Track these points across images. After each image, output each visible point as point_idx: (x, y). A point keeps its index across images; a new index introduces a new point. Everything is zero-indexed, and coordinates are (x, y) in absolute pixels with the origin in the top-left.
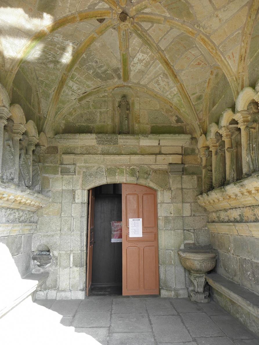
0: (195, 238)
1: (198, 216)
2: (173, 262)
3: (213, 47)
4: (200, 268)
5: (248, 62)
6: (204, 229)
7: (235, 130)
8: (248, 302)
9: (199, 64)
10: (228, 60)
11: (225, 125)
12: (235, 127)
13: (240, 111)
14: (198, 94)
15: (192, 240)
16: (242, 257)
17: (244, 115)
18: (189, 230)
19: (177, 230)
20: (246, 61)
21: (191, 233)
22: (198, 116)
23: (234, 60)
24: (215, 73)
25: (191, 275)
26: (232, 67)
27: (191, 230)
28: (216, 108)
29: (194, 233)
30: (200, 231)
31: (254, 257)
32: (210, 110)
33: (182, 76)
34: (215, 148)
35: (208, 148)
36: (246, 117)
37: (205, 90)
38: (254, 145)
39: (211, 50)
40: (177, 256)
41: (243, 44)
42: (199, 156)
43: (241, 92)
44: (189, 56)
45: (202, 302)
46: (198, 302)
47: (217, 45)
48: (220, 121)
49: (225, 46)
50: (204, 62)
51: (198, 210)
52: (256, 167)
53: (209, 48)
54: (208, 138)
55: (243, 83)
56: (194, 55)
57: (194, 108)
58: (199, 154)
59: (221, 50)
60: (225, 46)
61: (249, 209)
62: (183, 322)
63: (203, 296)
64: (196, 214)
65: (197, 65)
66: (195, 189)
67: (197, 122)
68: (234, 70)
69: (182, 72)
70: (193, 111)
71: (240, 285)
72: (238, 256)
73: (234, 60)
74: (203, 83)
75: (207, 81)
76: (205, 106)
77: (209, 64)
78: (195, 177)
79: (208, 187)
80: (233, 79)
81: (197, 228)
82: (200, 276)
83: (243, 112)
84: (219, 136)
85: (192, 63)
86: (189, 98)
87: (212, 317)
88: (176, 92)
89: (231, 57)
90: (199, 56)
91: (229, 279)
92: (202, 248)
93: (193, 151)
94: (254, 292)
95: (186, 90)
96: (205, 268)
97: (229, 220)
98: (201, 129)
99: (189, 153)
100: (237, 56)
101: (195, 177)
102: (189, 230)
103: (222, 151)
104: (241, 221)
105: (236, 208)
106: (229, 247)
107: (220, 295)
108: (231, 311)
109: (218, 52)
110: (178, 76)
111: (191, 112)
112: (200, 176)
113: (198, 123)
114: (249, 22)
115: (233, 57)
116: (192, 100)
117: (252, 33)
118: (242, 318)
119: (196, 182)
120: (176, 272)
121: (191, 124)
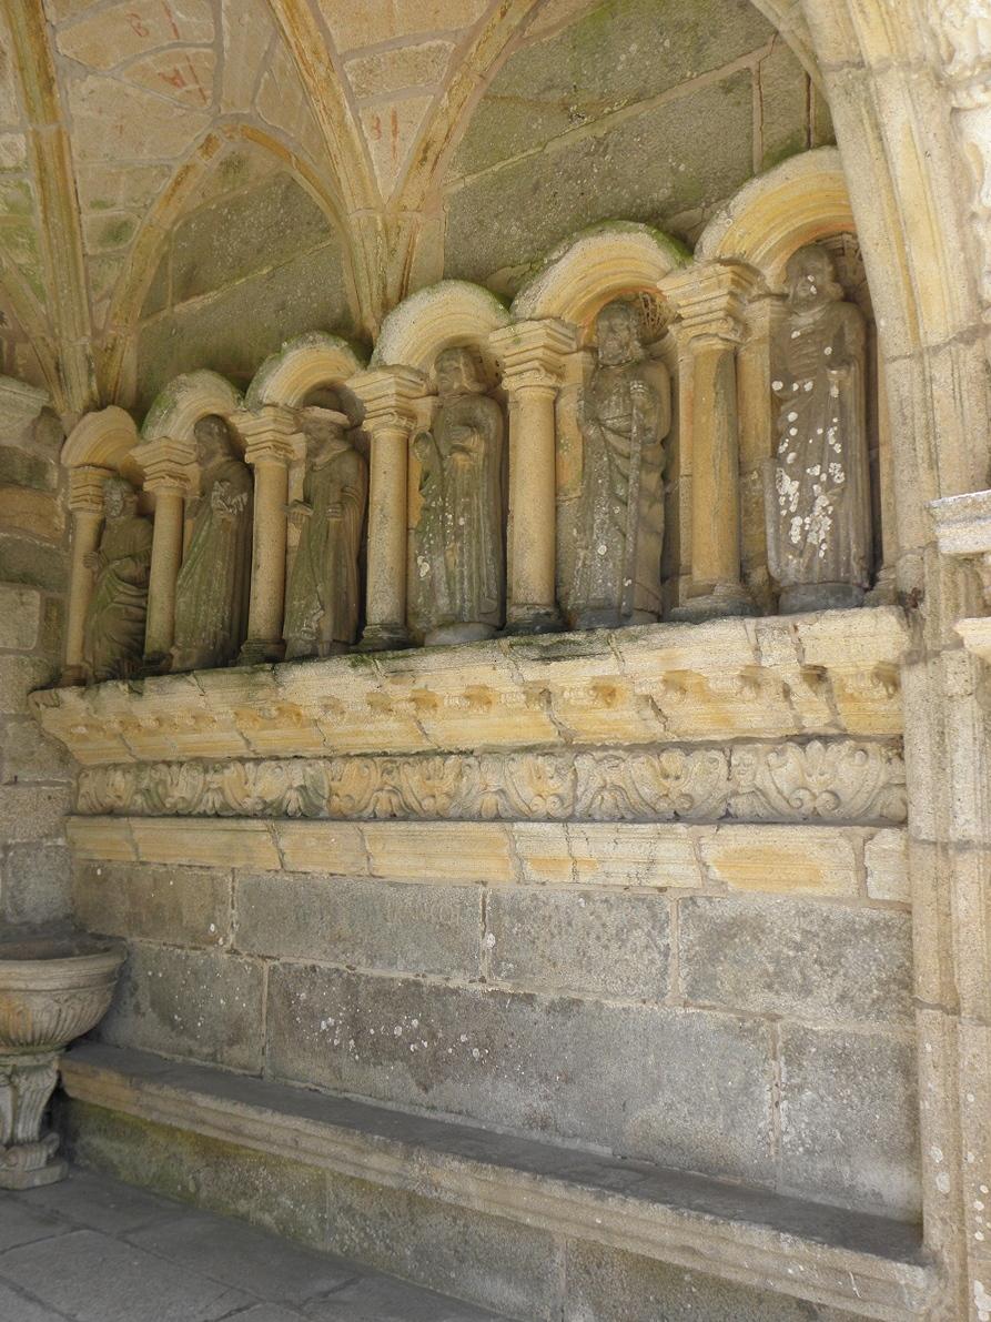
1: (29, 785)
3: (322, 48)
4: (52, 1026)
5: (456, 182)
6: (49, 844)
7: (331, 432)
8: (376, 1137)
9: (173, 79)
10: (366, 135)
11: (278, 398)
12: (332, 423)
13: (394, 366)
14: (117, 213)
16: (292, 960)
17: (404, 386)
20: (438, 170)
22: (90, 310)
23: (394, 148)
24: (225, 149)
26: (377, 173)
28: (205, 310)
30: (33, 852)
31: (368, 957)
32: (152, 307)
33: (80, 99)
34: (177, 483)
35: (132, 480)
36: (405, 397)
37: (151, 204)
38: (461, 519)
39: (309, 57)
41: (445, 102)
42: (59, 502)
43: (422, 294)
44: (150, 21)
45: (37, 1182)
46: (14, 1190)
47: (339, 51)
48: (262, 378)
49: (371, 71)
50: (202, 85)
51: (32, 753)
52: (462, 608)
53: (305, 44)
54: (153, 432)
55: (409, 253)
56: (176, 31)
57: (86, 269)
58: (63, 490)
59: (349, 77)
60: (371, 71)
61: (367, 767)
62: (31, 1298)
63: (39, 1156)
64: (25, 777)
65: (164, 78)
66: (27, 654)
67: (84, 340)
68: (385, 186)
69: (83, 81)
70: (78, 280)
71: (261, 1077)
72: (264, 958)
73: (394, 148)
74: (154, 173)
75: (175, 173)
76: (128, 278)
77: (217, 99)
78: (34, 598)
79: (112, 652)
80: (372, 221)
81: (19, 840)
82: (35, 1063)
83: (405, 375)
84: (217, 438)
85: (149, 60)
86: (75, 213)
87: (130, 1237)
88: (17, 159)
89: (383, 128)
90: (197, 46)
91: (192, 1059)
92: (34, 932)
93: (37, 469)
94: (348, 1095)
95: (73, 172)
96: (73, 1025)
97: (226, 806)
98: (94, 378)
99: (18, 478)
100: (410, 142)
101: (34, 598)
103: (230, 506)
104: (308, 815)
105: (278, 759)
106: (211, 919)
107: (133, 1130)
108: (203, 1194)
109: (334, 78)
110: (59, 89)
111: (70, 285)
112: (55, 595)
113: (84, 346)
114: (494, 26)
115: (395, 133)
116: (84, 229)
117: (493, 75)
118: (270, 1212)
119: (36, 623)
121: (43, 339)
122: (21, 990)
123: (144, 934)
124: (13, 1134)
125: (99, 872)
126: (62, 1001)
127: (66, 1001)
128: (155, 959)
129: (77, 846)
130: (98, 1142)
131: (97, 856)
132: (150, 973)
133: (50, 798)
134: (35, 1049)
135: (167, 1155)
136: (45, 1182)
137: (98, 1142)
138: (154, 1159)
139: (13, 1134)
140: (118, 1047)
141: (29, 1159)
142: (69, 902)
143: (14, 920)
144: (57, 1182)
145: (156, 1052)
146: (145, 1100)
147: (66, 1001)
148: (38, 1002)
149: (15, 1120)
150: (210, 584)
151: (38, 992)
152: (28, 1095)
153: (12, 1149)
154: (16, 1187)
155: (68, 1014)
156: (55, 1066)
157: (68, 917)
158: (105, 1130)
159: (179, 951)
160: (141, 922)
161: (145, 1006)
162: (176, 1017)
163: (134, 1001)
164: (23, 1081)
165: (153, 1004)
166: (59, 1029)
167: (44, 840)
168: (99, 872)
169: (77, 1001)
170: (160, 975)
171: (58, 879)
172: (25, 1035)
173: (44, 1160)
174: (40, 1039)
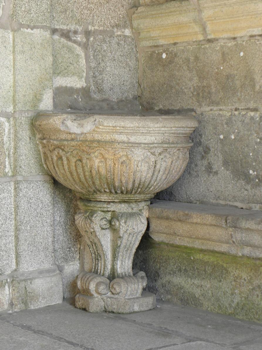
0: (89, 68)
2: (10, 163)
4: (150, 175)
6: (119, 33)
15: (80, 77)
18: (69, 31)
19: (28, 27)
21: (75, 46)
25: (93, 213)
27: (76, 32)
29: (85, 46)
30: (108, 39)
40: (28, 139)
45: (136, 308)
81: (96, 28)
82: (130, 211)
102: (71, 34)
120: (23, 205)
122: (124, 142)
123: (213, 103)
124: (113, 269)
125: (164, 56)
126: (157, 154)
127: (160, 154)
128: (227, 124)
129: (142, 35)
130: (178, 280)
131: (162, 42)
132: (222, 137)
134: (132, 197)
135: (251, 287)
136: (143, 309)
137: (178, 280)
138: (237, 291)
139: (113, 269)
140: (191, 202)
141: (129, 289)
142: (136, 85)
143: (97, 96)
144: (150, 310)
145: (231, 203)
146: (239, 236)
147: (160, 154)
148: (138, 154)
149: (115, 257)
151: (138, 145)
152: (126, 236)
153: (115, 280)
154: (121, 311)
155: (162, 165)
156: (146, 214)
157: (135, 98)
158: (185, 270)
159: (252, 114)
160: (209, 93)
161: (218, 164)
162: (251, 172)
163: (205, 162)
164: (123, 224)
165: (226, 163)
166: (154, 178)
167: (115, 30)
168: (164, 56)
169: (168, 156)
170: (233, 137)
171: (127, 64)
172: (127, 183)
173: (140, 291)
174: (138, 188)
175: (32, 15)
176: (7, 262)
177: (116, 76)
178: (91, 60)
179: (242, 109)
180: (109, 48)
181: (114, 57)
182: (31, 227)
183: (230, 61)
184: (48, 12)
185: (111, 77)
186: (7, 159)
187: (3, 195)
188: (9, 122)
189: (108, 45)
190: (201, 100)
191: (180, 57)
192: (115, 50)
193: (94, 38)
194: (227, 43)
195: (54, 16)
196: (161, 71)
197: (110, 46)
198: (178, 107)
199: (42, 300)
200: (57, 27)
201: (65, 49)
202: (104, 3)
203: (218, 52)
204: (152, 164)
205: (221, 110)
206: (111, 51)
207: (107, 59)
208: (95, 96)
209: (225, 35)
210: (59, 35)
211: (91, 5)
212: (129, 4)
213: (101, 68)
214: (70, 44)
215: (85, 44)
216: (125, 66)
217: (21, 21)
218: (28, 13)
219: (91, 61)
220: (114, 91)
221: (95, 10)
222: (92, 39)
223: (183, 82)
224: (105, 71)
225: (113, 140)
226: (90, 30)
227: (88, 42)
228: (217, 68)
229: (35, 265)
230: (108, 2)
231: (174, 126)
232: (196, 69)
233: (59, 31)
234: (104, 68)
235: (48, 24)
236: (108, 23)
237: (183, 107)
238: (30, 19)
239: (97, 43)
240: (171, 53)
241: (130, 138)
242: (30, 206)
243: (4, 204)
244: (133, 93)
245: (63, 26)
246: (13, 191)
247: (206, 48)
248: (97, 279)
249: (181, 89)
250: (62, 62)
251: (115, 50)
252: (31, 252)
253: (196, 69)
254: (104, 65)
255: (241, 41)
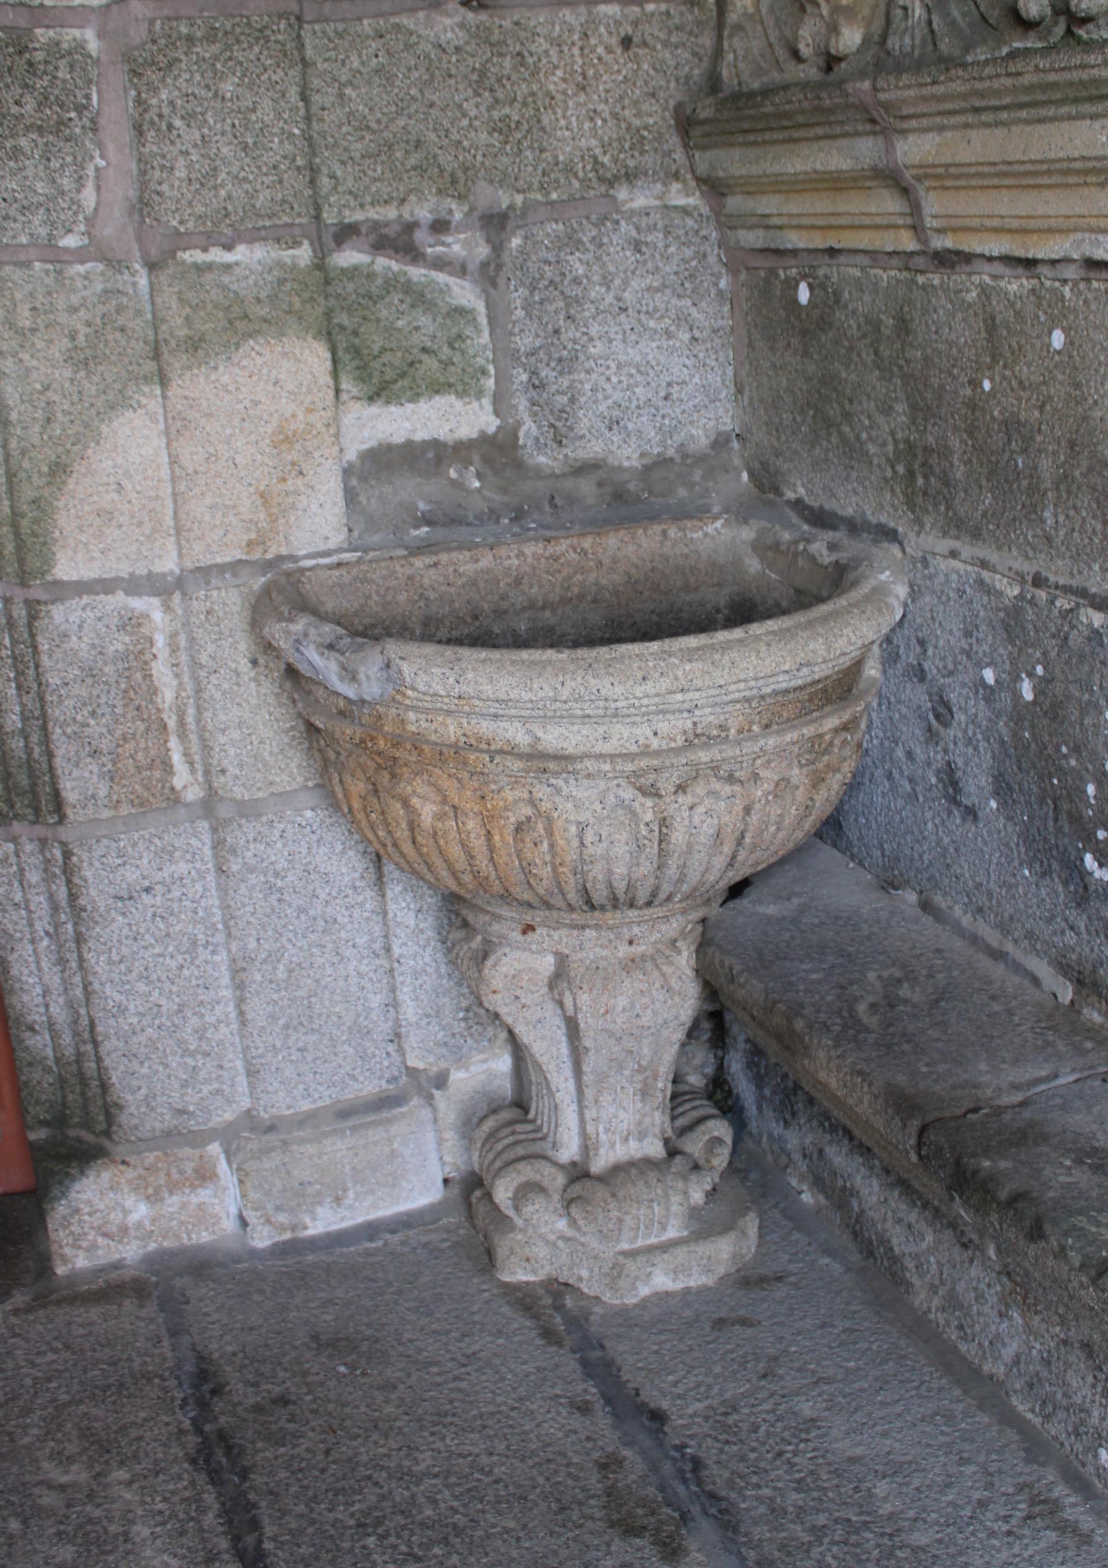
2: (186, 754)
4: (646, 868)
27: (440, 226)
40: (244, 665)
92: (619, 496)
102: (421, 236)
122: (512, 751)
125: (804, 295)
126: (666, 785)
133: (627, 42)
147: (681, 788)
150: (854, 1312)
168: (804, 295)
175: (223, 193)
176: (216, 1085)
177: (633, 371)
178: (514, 323)
179: (1057, 587)
180: (595, 267)
181: (619, 299)
182: (291, 971)
183: (1014, 361)
184: (298, 168)
185: (608, 379)
186: (174, 743)
187: (173, 868)
188: (167, 608)
189: (590, 256)
190: (920, 500)
191: (850, 308)
192: (625, 272)
193: (526, 238)
194: (1003, 277)
195: (339, 173)
196: (795, 353)
197: (598, 259)
198: (850, 510)
199: (356, 1200)
200: (359, 216)
201: (396, 297)
202: (564, 93)
203: (971, 312)
204: (644, 833)
205: (983, 564)
206: (604, 277)
207: (589, 310)
208: (542, 459)
209: (996, 246)
210: (367, 248)
211: (507, 110)
212: (682, 81)
213: (565, 348)
214: (417, 273)
215: (485, 265)
216: (673, 328)
217: (175, 223)
218: (202, 184)
219: (517, 330)
220: (626, 428)
221: (525, 127)
222: (516, 242)
223: (862, 413)
224: (582, 357)
225: (473, 742)
226: (504, 206)
227: (499, 256)
228: (970, 383)
229: (321, 1089)
230: (584, 88)
231: (735, 679)
232: (900, 368)
233: (363, 230)
234: (578, 347)
235: (299, 215)
236: (589, 167)
237: (864, 514)
238: (215, 205)
239: (543, 254)
240: (823, 286)
241: (540, 734)
242: (280, 900)
243: (181, 900)
244: (711, 424)
245: (381, 210)
246: (208, 852)
247: (933, 286)
248: (519, 1173)
249: (858, 438)
250: (383, 350)
251: (625, 272)
252: (299, 1050)
253: (900, 368)
254: (578, 335)
255: (1054, 280)
